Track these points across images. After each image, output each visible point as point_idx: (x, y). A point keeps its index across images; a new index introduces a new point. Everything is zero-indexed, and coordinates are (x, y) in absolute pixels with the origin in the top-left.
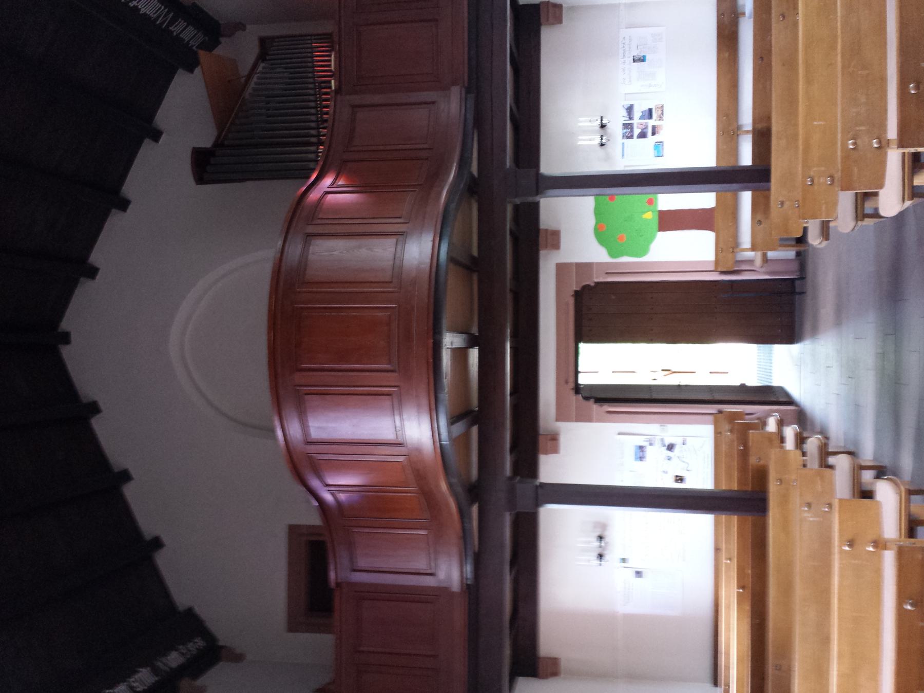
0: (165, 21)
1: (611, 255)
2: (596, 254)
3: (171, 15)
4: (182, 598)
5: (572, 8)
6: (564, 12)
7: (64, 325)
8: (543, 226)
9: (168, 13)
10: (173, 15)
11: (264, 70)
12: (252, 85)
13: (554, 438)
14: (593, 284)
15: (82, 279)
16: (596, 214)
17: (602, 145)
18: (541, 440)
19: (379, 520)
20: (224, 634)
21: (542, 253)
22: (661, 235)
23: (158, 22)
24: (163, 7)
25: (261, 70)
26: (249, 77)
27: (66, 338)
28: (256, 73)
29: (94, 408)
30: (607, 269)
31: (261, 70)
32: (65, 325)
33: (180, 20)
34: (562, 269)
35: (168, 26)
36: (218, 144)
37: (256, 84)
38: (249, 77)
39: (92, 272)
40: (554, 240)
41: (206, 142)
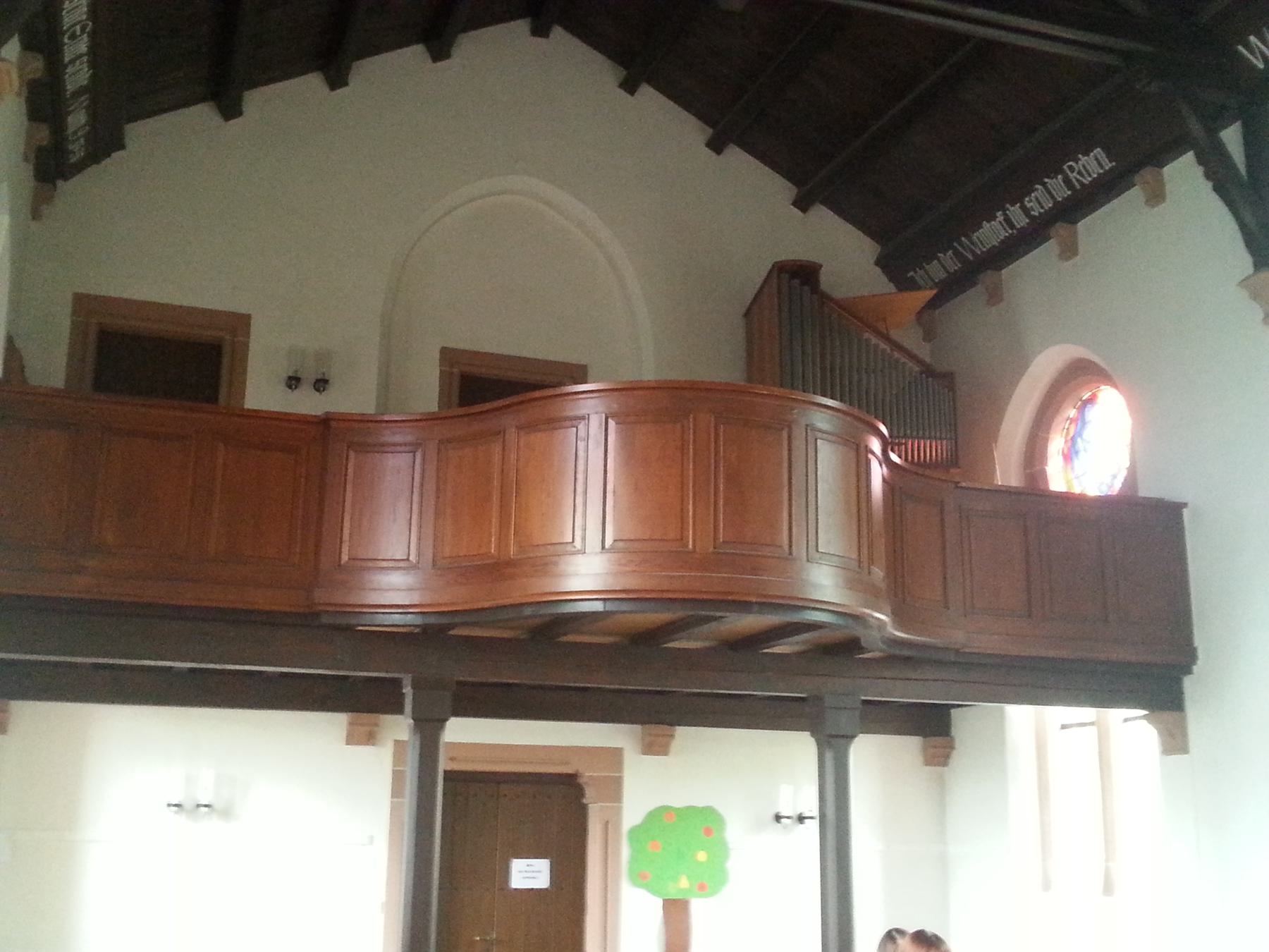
0: (963, 248)
1: (634, 831)
2: (633, 809)
3: (970, 257)
4: (139, 133)
5: (941, 787)
6: (938, 769)
7: (558, 32)
8: (681, 731)
9: (973, 252)
10: (968, 259)
11: (880, 353)
12: (874, 341)
13: (370, 738)
14: (584, 801)
15: (731, 145)
16: (688, 808)
17: (778, 818)
18: (365, 717)
19: (832, 562)
20: (69, 189)
21: (637, 728)
22: (660, 903)
23: (963, 239)
24: (985, 250)
25: (873, 343)
26: (887, 338)
27: (540, 31)
28: (892, 350)
29: (439, 52)
30: (611, 827)
31: (873, 343)
32: (558, 33)
33: (959, 265)
34: (614, 756)
35: (955, 250)
36: (825, 298)
37: (876, 346)
38: (887, 338)
39: (716, 145)
40: (655, 747)
41: (826, 281)
